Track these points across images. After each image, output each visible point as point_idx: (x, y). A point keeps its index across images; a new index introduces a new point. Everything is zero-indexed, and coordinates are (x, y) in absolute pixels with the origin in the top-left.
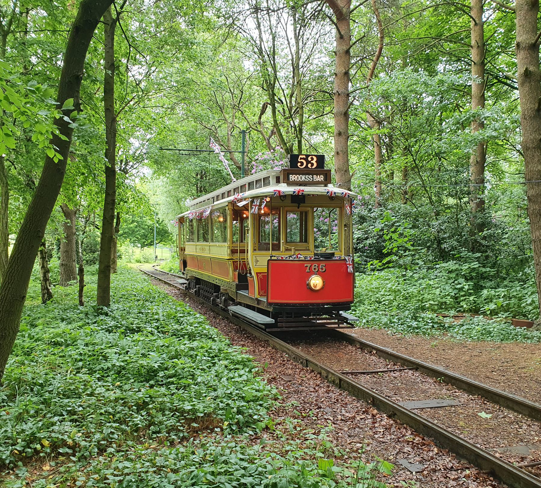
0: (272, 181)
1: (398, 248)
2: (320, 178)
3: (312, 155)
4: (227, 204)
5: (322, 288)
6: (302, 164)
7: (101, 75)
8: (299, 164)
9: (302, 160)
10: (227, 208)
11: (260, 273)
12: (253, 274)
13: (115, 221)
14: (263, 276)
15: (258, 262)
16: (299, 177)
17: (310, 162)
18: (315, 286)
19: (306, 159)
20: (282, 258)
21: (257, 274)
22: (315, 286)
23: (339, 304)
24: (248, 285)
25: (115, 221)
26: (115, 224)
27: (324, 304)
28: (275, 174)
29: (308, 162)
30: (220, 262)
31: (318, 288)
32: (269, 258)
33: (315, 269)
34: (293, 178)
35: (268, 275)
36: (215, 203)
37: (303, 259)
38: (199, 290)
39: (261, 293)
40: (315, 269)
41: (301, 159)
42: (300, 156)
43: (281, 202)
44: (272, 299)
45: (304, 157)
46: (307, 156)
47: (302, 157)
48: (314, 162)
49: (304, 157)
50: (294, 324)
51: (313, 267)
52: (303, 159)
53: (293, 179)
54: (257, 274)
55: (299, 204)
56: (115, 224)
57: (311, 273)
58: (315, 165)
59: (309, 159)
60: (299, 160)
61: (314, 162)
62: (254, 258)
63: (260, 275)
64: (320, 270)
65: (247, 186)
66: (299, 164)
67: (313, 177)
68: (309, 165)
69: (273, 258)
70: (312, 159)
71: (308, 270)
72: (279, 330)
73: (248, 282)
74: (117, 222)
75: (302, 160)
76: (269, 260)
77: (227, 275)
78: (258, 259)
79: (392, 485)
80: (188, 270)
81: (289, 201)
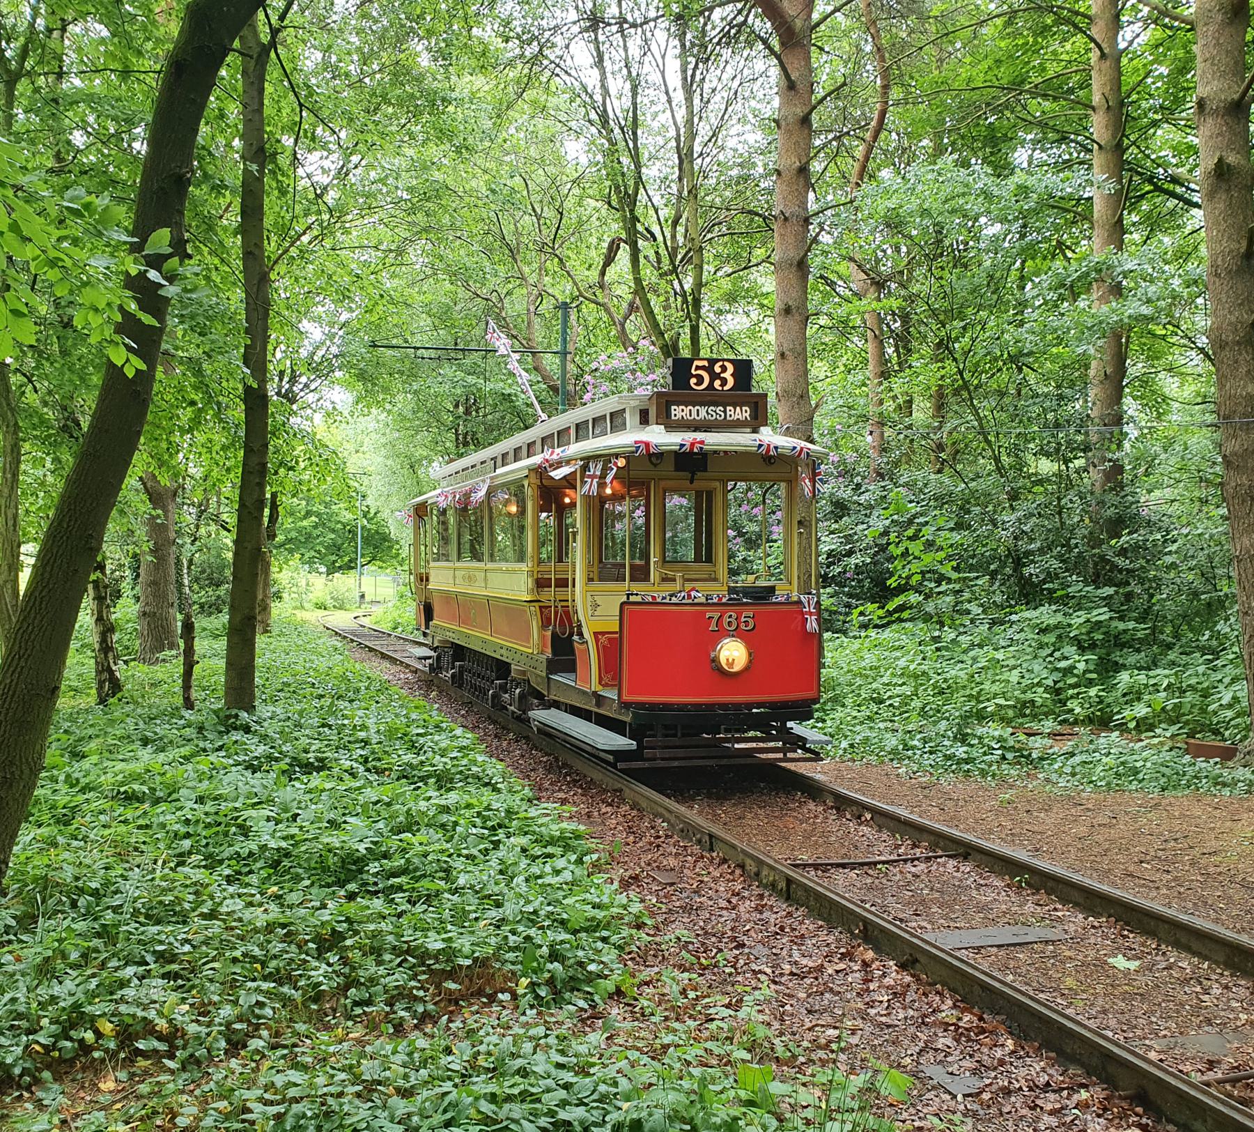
0: (631, 419)
1: (923, 576)
2: (743, 413)
3: (724, 360)
4: (526, 472)
5: (746, 669)
6: (700, 380)
7: (234, 175)
8: (693, 381)
9: (699, 372)
10: (526, 483)
11: (603, 633)
12: (587, 635)
13: (267, 512)
14: (610, 640)
15: (597, 609)
16: (694, 410)
17: (718, 376)
18: (731, 664)
19: (709, 369)
20: (654, 598)
21: (596, 634)
22: (731, 664)
23: (785, 705)
24: (574, 661)
25: (267, 512)
26: (266, 520)
27: (750, 706)
28: (637, 403)
29: (714, 376)
30: (509, 609)
31: (736, 668)
32: (624, 599)
33: (730, 624)
34: (678, 412)
35: (621, 637)
36: (499, 471)
37: (703, 600)
38: (461, 673)
39: (605, 680)
40: (730, 624)
41: (698, 368)
42: (696, 363)
43: (652, 468)
44: (629, 693)
45: (706, 363)
46: (712, 362)
47: (700, 363)
48: (727, 375)
49: (706, 363)
50: (680, 752)
51: (726, 619)
52: (703, 368)
53: (679, 416)
54: (596, 634)
55: (693, 474)
56: (266, 520)
57: (721, 633)
58: (731, 382)
59: (717, 369)
60: (693, 372)
61: (727, 375)
62: (589, 598)
63: (602, 639)
64: (743, 626)
65: (573, 432)
66: (693, 381)
67: (725, 412)
68: (717, 383)
69: (632, 599)
70: (724, 369)
71: (713, 627)
72: (647, 765)
73: (574, 654)
74: (271, 516)
75: (699, 372)
76: (623, 604)
77: (527, 637)
78: (599, 600)
79: (908, 1125)
80: (436, 627)
81: (669, 465)
